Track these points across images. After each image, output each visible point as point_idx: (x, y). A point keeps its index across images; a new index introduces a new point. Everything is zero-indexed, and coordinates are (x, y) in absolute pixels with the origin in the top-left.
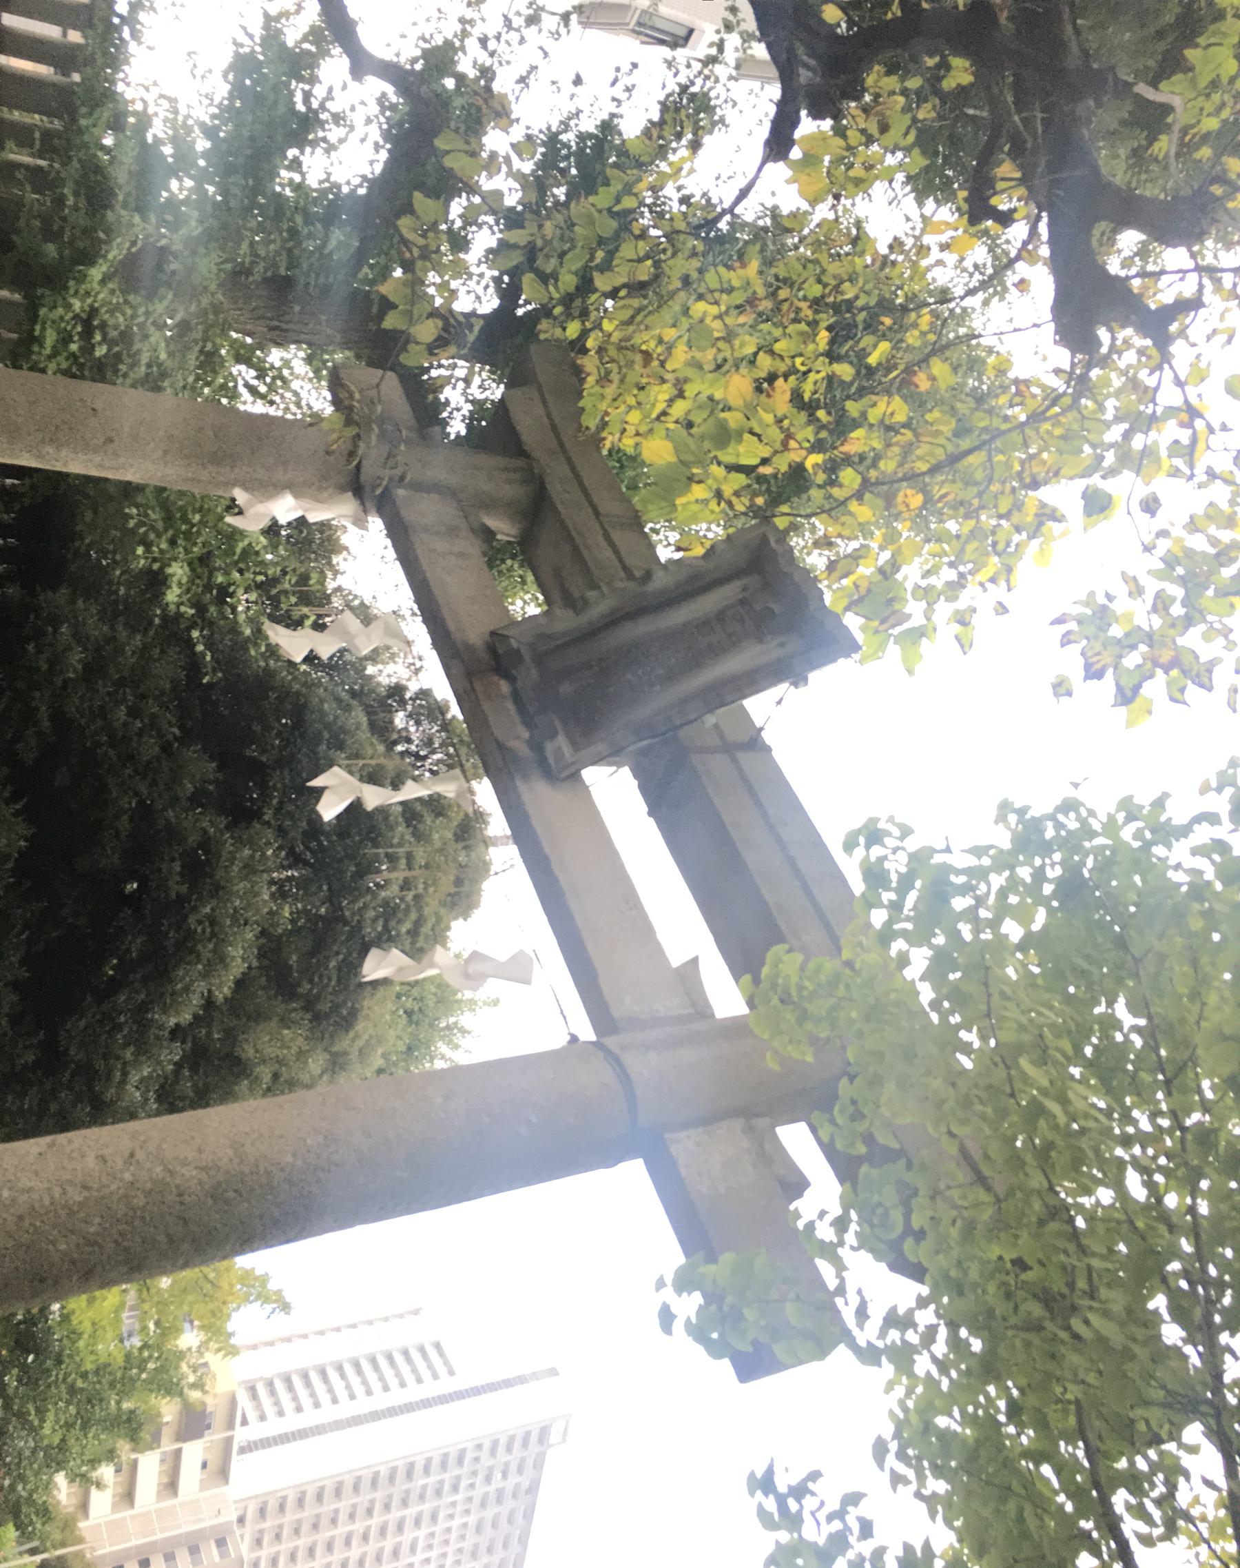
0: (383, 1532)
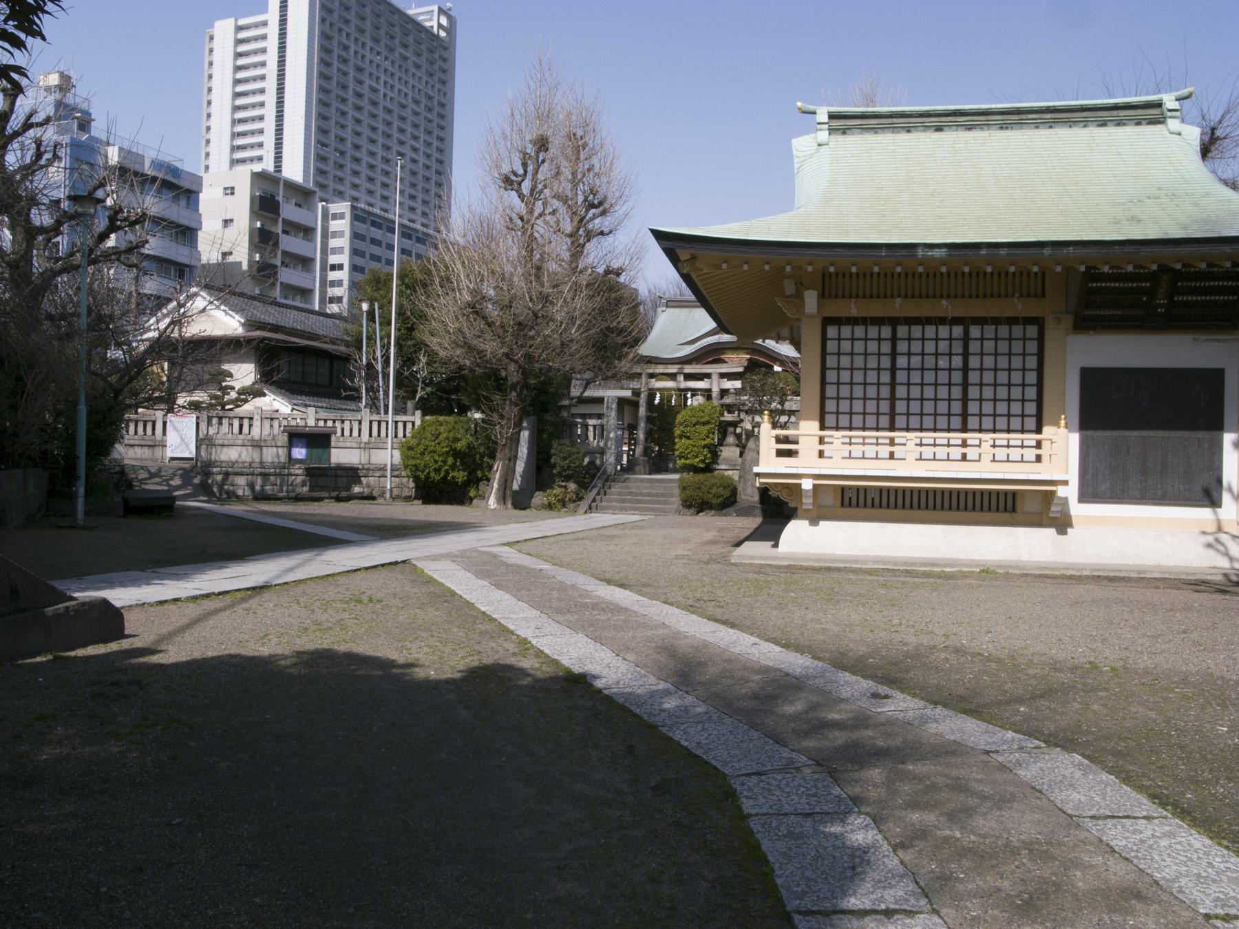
0: (358, 108)
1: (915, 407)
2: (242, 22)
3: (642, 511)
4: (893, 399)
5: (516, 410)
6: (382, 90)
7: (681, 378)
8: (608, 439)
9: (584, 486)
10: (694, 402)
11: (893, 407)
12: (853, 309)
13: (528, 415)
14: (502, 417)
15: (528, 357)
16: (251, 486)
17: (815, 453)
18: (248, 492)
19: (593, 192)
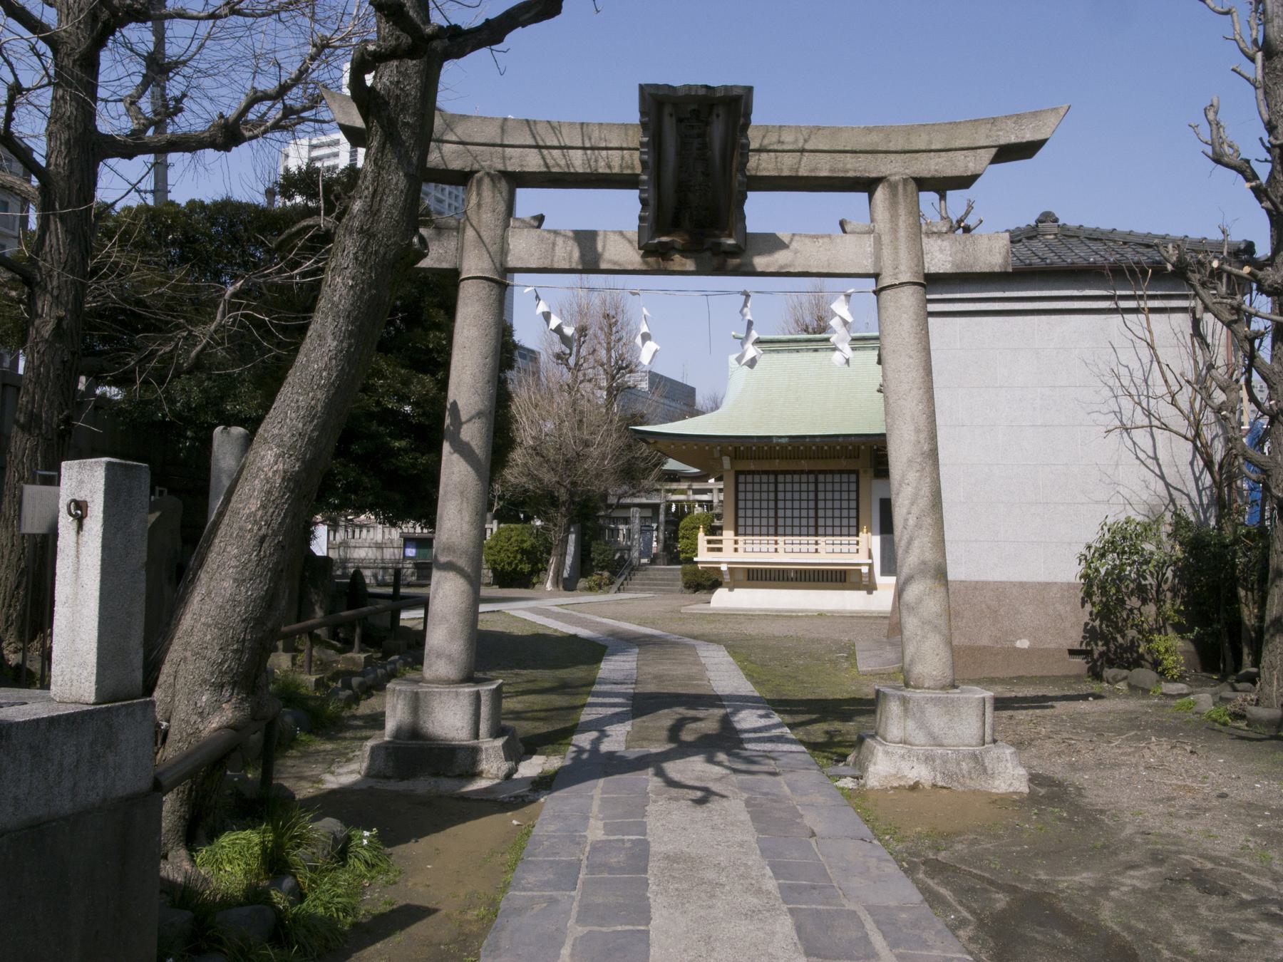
1: (789, 522)
2: (314, 142)
3: (656, 591)
4: (776, 517)
5: (565, 520)
6: (447, 201)
7: (690, 492)
9: (614, 573)
10: (698, 510)
11: (776, 522)
12: (752, 466)
14: (555, 525)
15: (574, 484)
16: (375, 576)
17: (731, 550)
18: (373, 581)
19: (621, 357)
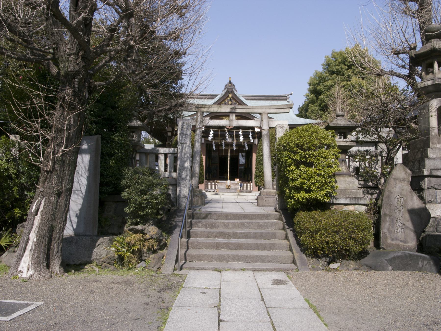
5: (71, 117)
7: (233, 117)
8: (183, 168)
9: (166, 227)
13: (89, 133)
